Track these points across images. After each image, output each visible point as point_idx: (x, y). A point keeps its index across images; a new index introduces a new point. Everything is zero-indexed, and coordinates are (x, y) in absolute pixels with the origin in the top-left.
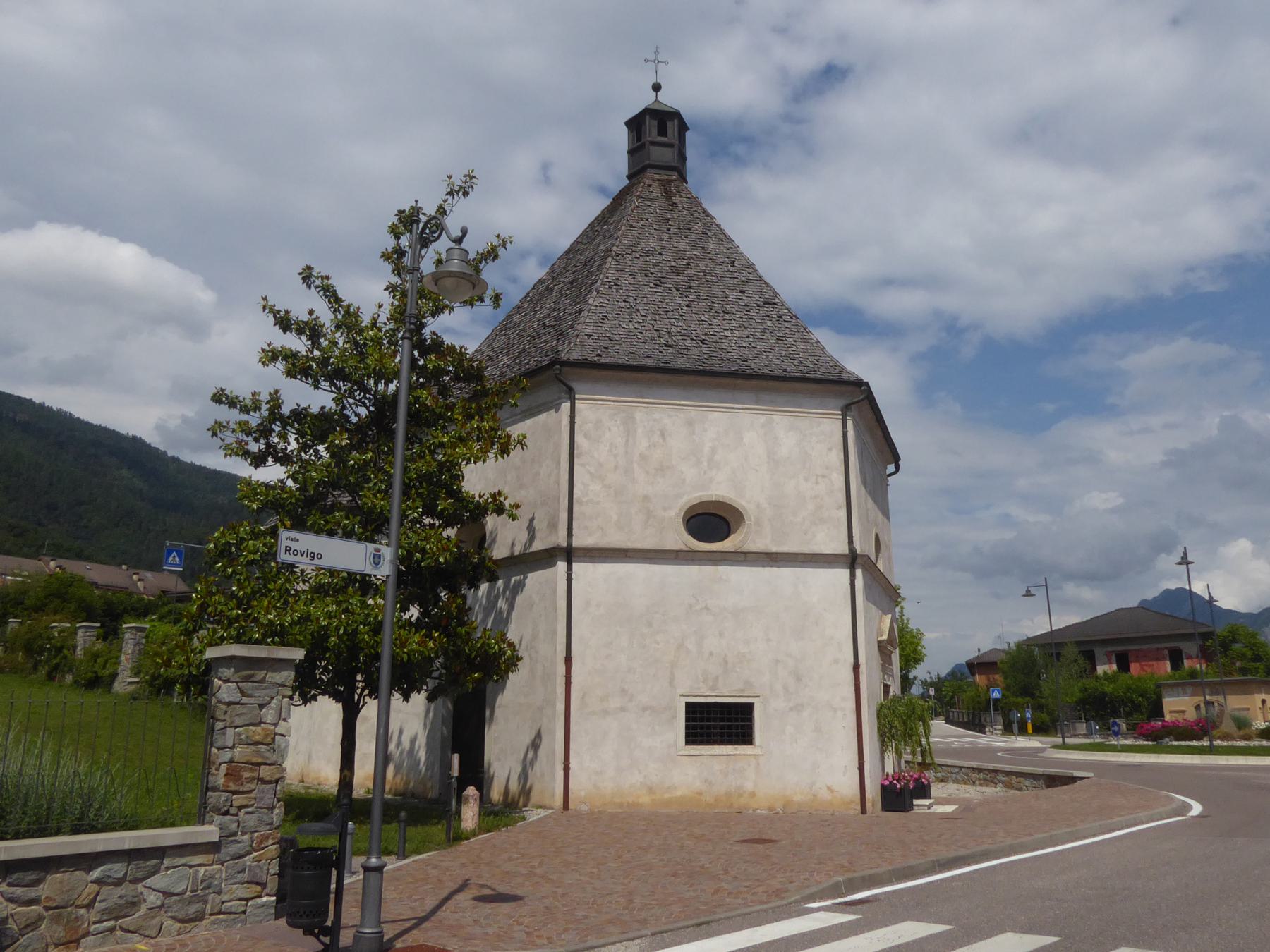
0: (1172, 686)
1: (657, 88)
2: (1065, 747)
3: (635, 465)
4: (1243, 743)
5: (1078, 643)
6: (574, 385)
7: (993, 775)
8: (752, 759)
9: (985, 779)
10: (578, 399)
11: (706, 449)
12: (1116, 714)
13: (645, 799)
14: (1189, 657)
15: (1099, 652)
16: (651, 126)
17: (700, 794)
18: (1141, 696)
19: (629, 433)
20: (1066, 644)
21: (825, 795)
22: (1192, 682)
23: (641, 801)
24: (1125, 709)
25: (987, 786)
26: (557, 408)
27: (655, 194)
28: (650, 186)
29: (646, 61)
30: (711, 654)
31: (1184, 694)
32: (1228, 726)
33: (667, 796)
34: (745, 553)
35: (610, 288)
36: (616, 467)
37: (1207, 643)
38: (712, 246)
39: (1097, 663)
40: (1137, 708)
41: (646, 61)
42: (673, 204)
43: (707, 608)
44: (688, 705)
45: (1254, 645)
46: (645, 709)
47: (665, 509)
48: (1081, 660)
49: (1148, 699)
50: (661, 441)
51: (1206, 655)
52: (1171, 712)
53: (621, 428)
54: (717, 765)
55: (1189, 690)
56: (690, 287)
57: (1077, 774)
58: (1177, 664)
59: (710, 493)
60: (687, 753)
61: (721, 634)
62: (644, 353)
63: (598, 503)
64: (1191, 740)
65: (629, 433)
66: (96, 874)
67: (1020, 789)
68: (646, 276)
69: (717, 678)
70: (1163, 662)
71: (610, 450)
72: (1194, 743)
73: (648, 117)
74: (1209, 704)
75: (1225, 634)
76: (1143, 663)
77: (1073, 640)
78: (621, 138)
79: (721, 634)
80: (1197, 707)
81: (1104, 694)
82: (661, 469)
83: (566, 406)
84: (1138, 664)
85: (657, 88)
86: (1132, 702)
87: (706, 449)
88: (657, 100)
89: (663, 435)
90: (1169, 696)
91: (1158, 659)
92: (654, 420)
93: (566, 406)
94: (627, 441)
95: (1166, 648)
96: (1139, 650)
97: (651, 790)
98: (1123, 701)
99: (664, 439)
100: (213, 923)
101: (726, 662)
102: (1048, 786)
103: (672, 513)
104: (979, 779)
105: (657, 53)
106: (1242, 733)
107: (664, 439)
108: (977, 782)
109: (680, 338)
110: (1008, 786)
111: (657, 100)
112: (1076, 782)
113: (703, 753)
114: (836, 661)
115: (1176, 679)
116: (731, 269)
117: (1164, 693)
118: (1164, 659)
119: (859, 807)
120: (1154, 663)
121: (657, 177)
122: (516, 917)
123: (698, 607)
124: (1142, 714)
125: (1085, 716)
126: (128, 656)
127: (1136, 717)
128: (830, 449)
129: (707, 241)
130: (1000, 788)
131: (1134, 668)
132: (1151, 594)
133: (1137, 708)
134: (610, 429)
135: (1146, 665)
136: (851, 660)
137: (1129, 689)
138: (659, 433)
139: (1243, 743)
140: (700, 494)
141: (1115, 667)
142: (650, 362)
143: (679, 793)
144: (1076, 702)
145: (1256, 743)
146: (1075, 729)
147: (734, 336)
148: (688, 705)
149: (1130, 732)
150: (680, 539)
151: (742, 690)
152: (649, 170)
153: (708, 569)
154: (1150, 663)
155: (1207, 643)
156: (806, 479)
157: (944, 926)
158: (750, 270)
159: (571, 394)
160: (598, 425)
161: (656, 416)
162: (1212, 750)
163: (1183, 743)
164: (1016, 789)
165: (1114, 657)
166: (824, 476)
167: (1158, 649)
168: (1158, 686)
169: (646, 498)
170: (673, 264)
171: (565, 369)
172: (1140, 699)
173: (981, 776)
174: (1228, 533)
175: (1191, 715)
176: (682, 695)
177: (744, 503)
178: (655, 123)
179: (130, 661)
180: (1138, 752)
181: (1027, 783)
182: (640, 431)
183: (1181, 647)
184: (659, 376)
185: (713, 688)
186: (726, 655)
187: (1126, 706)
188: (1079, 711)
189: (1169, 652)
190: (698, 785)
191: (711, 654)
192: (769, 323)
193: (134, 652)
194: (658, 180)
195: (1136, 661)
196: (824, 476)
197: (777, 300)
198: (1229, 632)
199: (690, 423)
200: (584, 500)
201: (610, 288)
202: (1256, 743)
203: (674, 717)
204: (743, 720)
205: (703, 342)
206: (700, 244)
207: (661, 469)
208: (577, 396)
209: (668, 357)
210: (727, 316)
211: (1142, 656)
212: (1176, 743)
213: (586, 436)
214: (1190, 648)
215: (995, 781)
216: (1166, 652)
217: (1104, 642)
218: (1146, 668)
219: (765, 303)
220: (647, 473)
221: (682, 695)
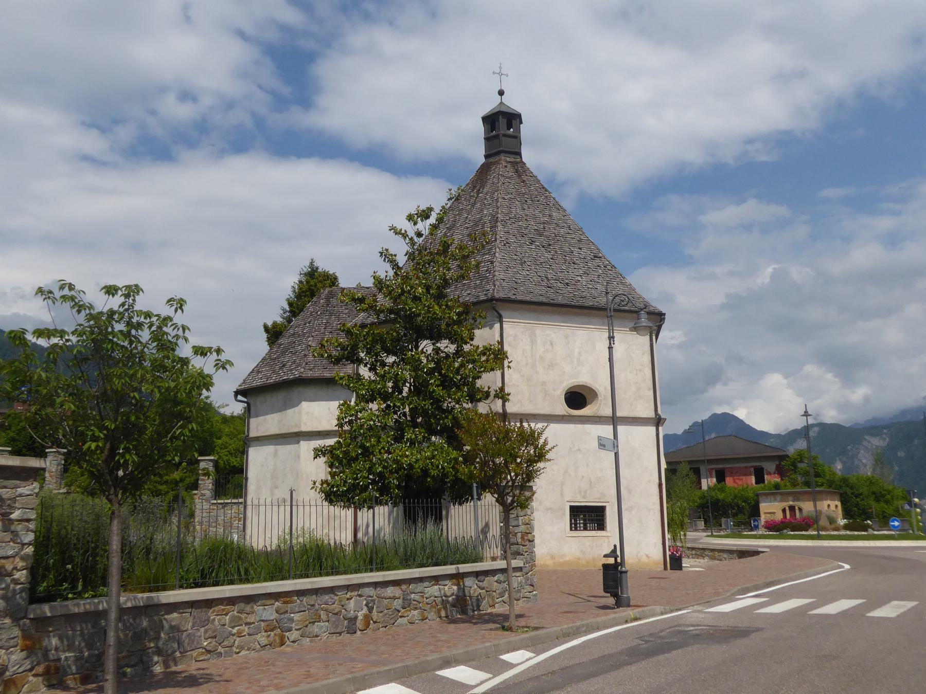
0: (766, 495)
1: (501, 93)
2: (712, 536)
3: (537, 363)
4: (836, 533)
5: (690, 462)
6: (501, 312)
7: (702, 551)
8: (606, 539)
9: (696, 554)
10: (505, 322)
11: (576, 354)
12: (725, 514)
13: (550, 562)
14: (769, 473)
15: (703, 470)
16: (502, 122)
17: (579, 559)
18: (745, 501)
19: (533, 343)
20: (681, 462)
21: (645, 559)
22: (776, 491)
23: (547, 563)
24: (733, 511)
25: (698, 558)
26: (491, 327)
27: (511, 174)
28: (506, 167)
29: (494, 73)
30: (583, 477)
31: (775, 500)
32: (823, 522)
33: (561, 560)
34: (599, 417)
35: (505, 245)
36: (527, 364)
37: (783, 463)
38: (554, 214)
39: (702, 477)
40: (740, 510)
41: (494, 73)
42: (523, 181)
43: (579, 450)
44: (571, 507)
45: (815, 465)
46: (548, 509)
47: (554, 390)
48: (692, 475)
49: (749, 504)
50: (551, 348)
51: (780, 471)
52: (765, 513)
53: (529, 340)
54: (588, 542)
55: (778, 498)
56: (550, 245)
57: (760, 549)
58: (760, 480)
59: (579, 380)
60: (571, 535)
61: (587, 465)
62: (538, 292)
63: (518, 386)
64: (802, 531)
65: (533, 343)
66: (496, 578)
67: (720, 560)
68: (523, 236)
69: (586, 492)
70: (749, 477)
71: (523, 354)
72: (804, 533)
73: (500, 117)
74: (792, 508)
75: (796, 457)
76: (735, 477)
77: (687, 459)
78: (479, 129)
79: (587, 465)
80: (784, 511)
81: (718, 500)
82: (552, 365)
83: (497, 326)
84: (731, 478)
85: (501, 93)
86: (738, 506)
87: (576, 354)
88: (501, 103)
89: (551, 344)
90: (765, 502)
91: (746, 475)
92: (547, 335)
93: (497, 326)
94: (532, 348)
95: (752, 467)
96: (732, 468)
97: (552, 557)
98: (731, 505)
99: (552, 347)
100: (524, 601)
101: (591, 483)
102: (740, 558)
103: (559, 392)
104: (692, 554)
105: (500, 68)
106: (833, 526)
107: (552, 347)
108: (691, 556)
109: (553, 281)
110: (712, 558)
111: (501, 103)
112: (759, 554)
113: (580, 535)
114: (649, 481)
115: (767, 490)
116: (570, 232)
117: (761, 499)
118: (751, 475)
119: (663, 567)
120: (744, 477)
121: (508, 159)
122: (273, 676)
123: (575, 449)
124: (744, 514)
125: (703, 516)
126: (52, 474)
127: (741, 517)
128: (643, 354)
129: (550, 210)
130: (706, 560)
131: (729, 481)
132: (705, 416)
133: (740, 510)
134: (522, 340)
135: (738, 479)
136: (657, 481)
137: (736, 497)
138: (549, 343)
139: (836, 533)
140: (575, 380)
141: (714, 480)
142: (544, 300)
143: (567, 559)
144: (697, 506)
145: (843, 533)
146: (696, 525)
147: (584, 280)
148: (571, 507)
149: (736, 528)
150: (562, 408)
151: (599, 498)
152: (502, 154)
153: (579, 426)
154: (741, 477)
155: (783, 463)
156: (630, 372)
157: (800, 600)
158: (581, 233)
159: (500, 319)
160: (516, 337)
161: (547, 332)
162: (818, 537)
163: (797, 533)
164: (718, 560)
165: (714, 473)
166: (640, 370)
167: (746, 467)
168: (757, 495)
169: (544, 383)
170: (536, 228)
171: (498, 303)
172: (744, 504)
173: (694, 552)
174: (759, 369)
175: (779, 516)
176: (568, 501)
177: (598, 387)
178: (505, 121)
179: (54, 477)
180: (772, 539)
181: (725, 556)
182: (539, 341)
183: (763, 466)
184: (550, 308)
185: (584, 497)
186: (590, 478)
187: (734, 509)
188: (699, 512)
189: (755, 469)
190: (578, 554)
191: (583, 477)
192: (600, 271)
193: (57, 470)
194: (510, 162)
195: (730, 476)
196: (640, 370)
197: (600, 255)
198: (799, 455)
199: (566, 337)
200: (510, 384)
201: (505, 245)
202: (843, 533)
203: (564, 514)
204: (599, 516)
205: (567, 284)
206: (547, 213)
207: (552, 365)
208: (504, 320)
209: (552, 296)
210: (576, 266)
211: (734, 473)
212: (792, 533)
213: (510, 345)
214: (770, 466)
215: (704, 555)
216: (752, 470)
217: (710, 462)
218: (737, 481)
219: (595, 257)
220: (544, 368)
221: (568, 501)
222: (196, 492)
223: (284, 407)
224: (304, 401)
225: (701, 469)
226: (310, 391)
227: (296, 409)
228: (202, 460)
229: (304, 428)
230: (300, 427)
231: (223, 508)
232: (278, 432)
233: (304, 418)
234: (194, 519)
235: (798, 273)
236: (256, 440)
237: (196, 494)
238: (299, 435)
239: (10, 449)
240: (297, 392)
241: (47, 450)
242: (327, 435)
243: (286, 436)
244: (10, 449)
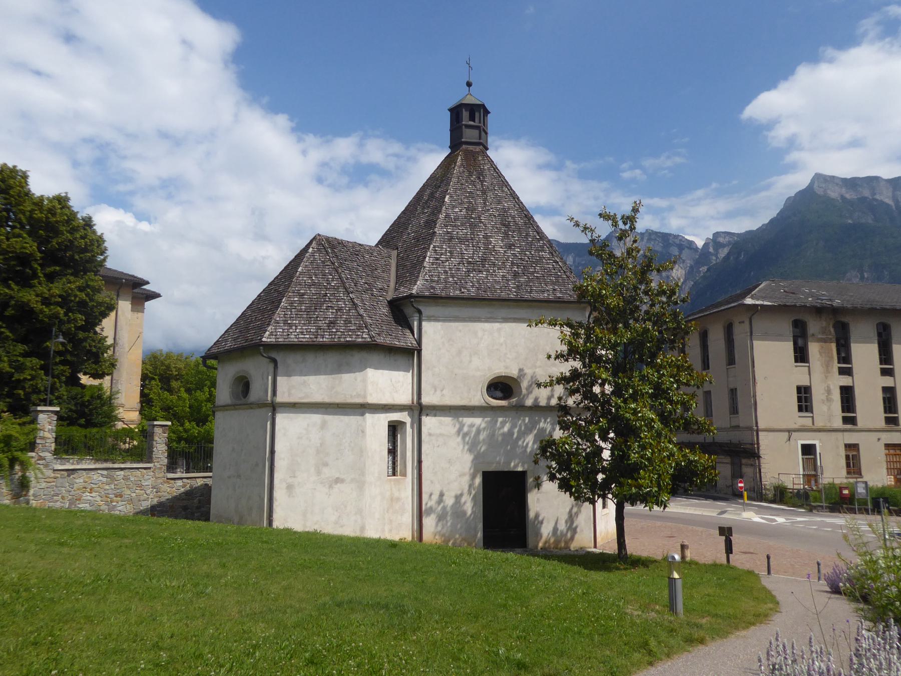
1: (469, 84)
6: (420, 308)
73: (464, 110)
85: (469, 84)
222: (33, 454)
223: (339, 369)
224: (370, 368)
225: (844, 472)
226: (375, 357)
227: (358, 375)
228: (42, 412)
229: (372, 399)
230: (365, 397)
231: (69, 476)
232: (327, 400)
233: (370, 388)
234: (28, 491)
235: (78, 283)
236: (288, 407)
237: (32, 457)
238: (365, 408)
239: (58, 409)
240: (357, 357)
241: (39, 408)
242: (390, 409)
243: (344, 406)
244: (169, 423)
